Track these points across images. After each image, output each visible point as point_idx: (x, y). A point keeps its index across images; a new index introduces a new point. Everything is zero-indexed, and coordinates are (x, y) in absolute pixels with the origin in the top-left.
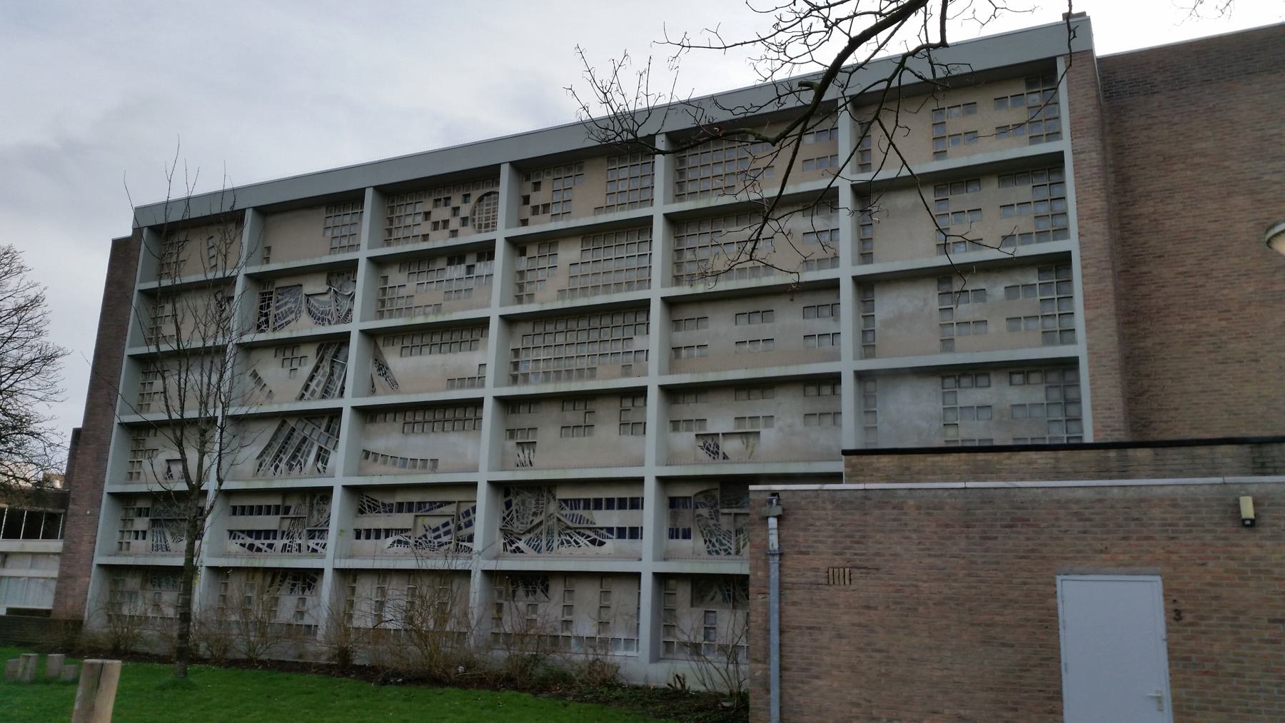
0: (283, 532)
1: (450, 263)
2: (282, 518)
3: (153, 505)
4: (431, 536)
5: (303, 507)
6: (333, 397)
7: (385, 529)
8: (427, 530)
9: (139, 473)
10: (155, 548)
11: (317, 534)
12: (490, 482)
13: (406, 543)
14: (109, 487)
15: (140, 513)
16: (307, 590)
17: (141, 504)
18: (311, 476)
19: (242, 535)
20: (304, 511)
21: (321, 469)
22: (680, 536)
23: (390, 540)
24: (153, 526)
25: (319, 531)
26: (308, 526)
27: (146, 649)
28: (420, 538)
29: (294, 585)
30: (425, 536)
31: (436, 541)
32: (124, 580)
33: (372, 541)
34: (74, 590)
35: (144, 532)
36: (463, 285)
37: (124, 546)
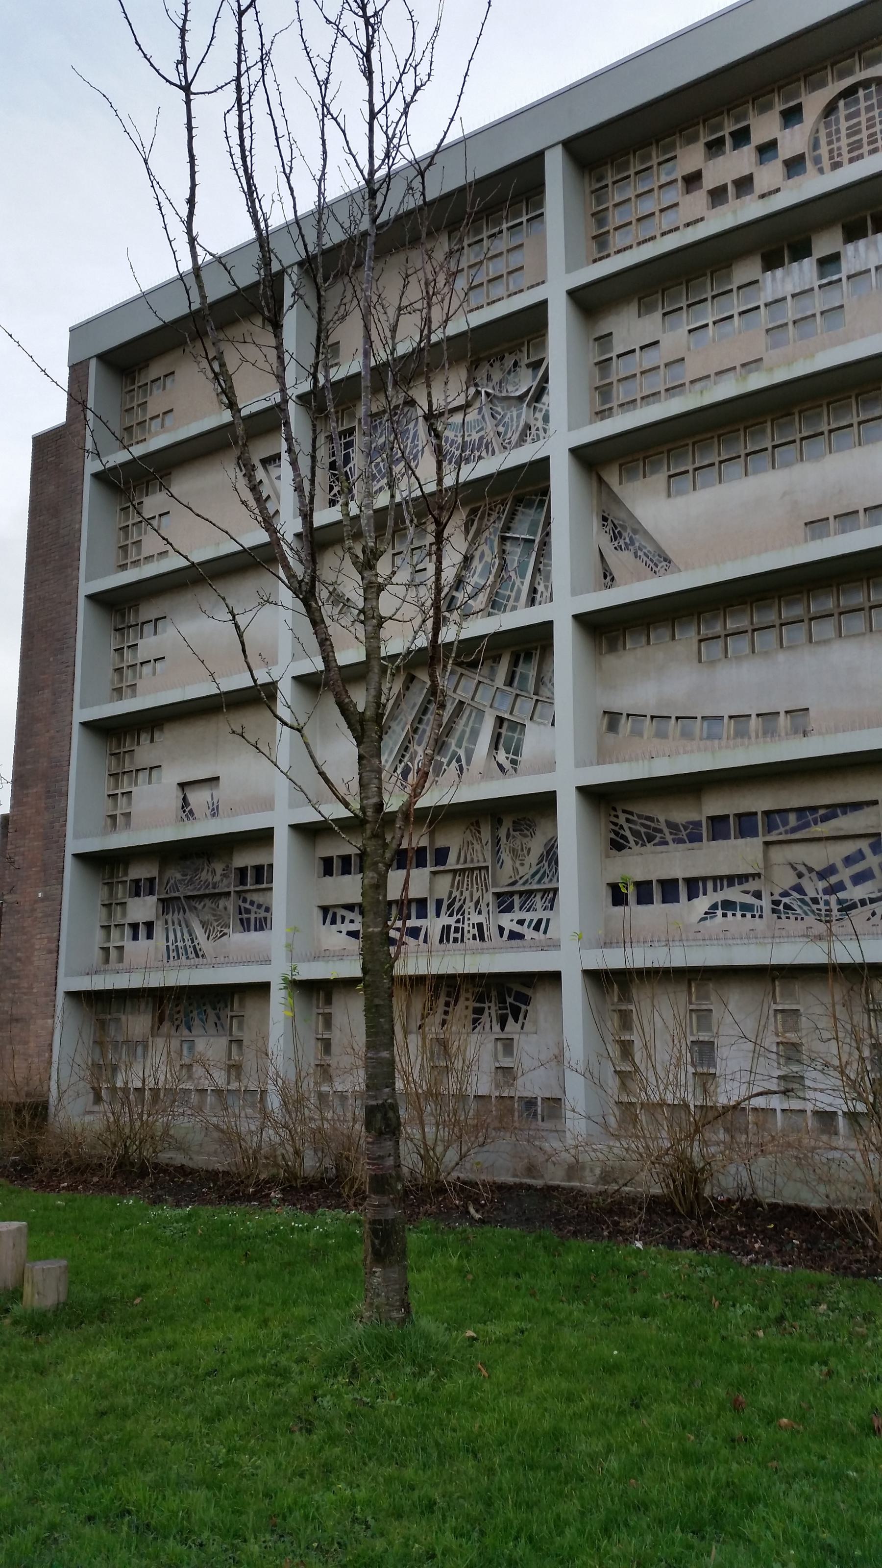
0: (439, 903)
1: (772, 262)
2: (434, 873)
3: (161, 873)
4: (813, 887)
5: (477, 847)
6: (504, 611)
7: (658, 881)
8: (800, 875)
9: (128, 815)
10: (173, 954)
11: (517, 900)
12: (581, 790)
13: (746, 908)
14: (74, 845)
15: (136, 889)
16: (510, 1020)
17: (139, 872)
18: (484, 776)
19: (349, 915)
20: (482, 855)
21: (507, 765)
22: (252, 927)
23: (702, 904)
24: (165, 911)
25: (521, 893)
26: (495, 885)
27: (179, 1159)
28: (785, 894)
29: (479, 1011)
30: (799, 889)
31: (833, 899)
32: (118, 1020)
33: (657, 910)
34: (26, 1043)
35: (149, 926)
36: (818, 303)
37: (113, 954)
